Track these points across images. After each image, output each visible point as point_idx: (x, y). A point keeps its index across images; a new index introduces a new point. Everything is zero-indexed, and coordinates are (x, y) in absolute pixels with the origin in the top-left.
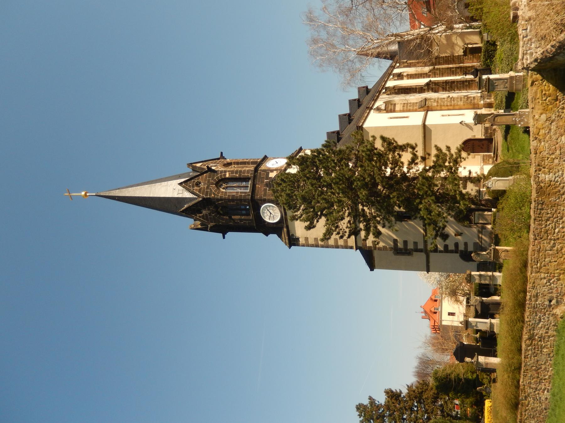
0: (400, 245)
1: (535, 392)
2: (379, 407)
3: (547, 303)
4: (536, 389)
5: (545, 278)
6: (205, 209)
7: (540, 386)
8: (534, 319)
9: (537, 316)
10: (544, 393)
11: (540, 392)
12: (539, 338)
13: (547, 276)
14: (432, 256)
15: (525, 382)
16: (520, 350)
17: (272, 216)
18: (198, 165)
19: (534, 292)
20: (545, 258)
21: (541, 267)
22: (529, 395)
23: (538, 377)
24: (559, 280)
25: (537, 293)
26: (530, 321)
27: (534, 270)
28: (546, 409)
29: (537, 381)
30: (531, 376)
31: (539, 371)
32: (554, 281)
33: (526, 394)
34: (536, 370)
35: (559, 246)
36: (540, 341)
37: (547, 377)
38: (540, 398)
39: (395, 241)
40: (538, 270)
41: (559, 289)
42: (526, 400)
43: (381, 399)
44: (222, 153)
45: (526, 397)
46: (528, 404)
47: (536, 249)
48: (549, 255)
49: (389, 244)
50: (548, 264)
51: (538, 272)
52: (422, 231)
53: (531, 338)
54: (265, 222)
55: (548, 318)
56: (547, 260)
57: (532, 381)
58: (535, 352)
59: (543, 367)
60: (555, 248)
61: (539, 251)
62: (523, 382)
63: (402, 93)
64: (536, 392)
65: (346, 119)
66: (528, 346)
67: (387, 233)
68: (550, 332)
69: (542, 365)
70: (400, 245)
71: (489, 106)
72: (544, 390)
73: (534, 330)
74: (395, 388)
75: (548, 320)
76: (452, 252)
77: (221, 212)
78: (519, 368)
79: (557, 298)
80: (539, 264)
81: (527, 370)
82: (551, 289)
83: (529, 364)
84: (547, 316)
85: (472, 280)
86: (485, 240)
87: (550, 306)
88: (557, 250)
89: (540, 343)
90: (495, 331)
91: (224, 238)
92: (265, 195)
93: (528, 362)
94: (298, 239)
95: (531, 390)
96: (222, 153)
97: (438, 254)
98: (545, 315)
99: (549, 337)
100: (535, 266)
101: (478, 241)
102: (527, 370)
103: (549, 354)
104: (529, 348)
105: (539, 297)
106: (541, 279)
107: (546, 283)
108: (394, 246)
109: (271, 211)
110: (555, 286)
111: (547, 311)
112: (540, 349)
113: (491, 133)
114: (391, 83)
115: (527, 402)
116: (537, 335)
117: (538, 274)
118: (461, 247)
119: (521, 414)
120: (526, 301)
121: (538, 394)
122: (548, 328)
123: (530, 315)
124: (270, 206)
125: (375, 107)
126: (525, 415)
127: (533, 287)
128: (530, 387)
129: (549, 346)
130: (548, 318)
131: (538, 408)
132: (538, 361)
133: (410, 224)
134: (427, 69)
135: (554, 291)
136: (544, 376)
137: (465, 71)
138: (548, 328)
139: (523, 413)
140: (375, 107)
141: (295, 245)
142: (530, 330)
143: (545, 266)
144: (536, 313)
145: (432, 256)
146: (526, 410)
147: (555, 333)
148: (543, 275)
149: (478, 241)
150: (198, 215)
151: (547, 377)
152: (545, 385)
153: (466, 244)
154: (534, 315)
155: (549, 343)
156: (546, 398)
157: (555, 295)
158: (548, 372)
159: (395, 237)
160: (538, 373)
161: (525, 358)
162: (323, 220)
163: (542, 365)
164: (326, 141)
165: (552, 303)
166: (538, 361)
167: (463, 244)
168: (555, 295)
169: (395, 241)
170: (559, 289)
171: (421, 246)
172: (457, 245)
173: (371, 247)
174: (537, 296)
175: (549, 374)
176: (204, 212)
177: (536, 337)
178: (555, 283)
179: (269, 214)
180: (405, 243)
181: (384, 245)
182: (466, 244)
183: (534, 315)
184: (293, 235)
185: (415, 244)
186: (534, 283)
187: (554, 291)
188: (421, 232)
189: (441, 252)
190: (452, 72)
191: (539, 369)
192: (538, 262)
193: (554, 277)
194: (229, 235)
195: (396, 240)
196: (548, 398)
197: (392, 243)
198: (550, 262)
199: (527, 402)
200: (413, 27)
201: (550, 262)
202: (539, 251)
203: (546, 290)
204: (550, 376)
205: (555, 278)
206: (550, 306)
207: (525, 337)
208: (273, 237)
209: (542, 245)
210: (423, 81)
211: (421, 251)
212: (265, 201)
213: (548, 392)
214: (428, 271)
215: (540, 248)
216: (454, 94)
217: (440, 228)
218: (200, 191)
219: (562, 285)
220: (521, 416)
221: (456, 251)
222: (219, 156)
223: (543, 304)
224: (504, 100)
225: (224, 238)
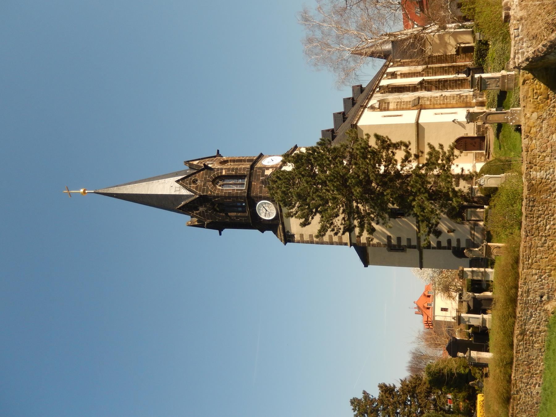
0: (394, 242)
1: (526, 386)
2: (373, 401)
3: (538, 299)
4: (528, 383)
5: (536, 274)
6: (201, 206)
7: (531, 380)
8: (525, 314)
9: (528, 311)
10: (535, 387)
11: (532, 387)
12: (530, 333)
13: (539, 272)
14: (426, 252)
15: (517, 377)
16: (512, 345)
17: (267, 213)
18: (195, 163)
19: (525, 288)
20: (536, 255)
21: (532, 264)
22: (520, 390)
23: (530, 372)
24: (550, 276)
25: (529, 289)
26: (521, 317)
27: (525, 266)
28: (537, 403)
29: (528, 376)
30: (522, 371)
31: (530, 366)
32: (545, 277)
33: (518, 388)
34: (528, 365)
35: (550, 243)
36: (532, 336)
37: (538, 372)
38: (532, 392)
39: (389, 238)
40: (529, 266)
41: (551, 285)
42: (517, 394)
43: (375, 393)
44: (218, 151)
45: (517, 392)
46: (520, 398)
47: (528, 245)
48: (540, 252)
49: (383, 241)
50: (539, 260)
51: (530, 268)
52: (415, 228)
53: (523, 333)
54: (261, 218)
55: (540, 313)
56: (538, 256)
57: (524, 376)
58: (526, 347)
59: (535, 362)
60: (546, 245)
61: (530, 248)
62: (514, 377)
63: (395, 92)
64: (528, 387)
65: (341, 118)
66: (520, 342)
67: (381, 230)
68: (542, 328)
69: (533, 359)
70: (394, 242)
71: (482, 104)
72: (536, 384)
73: (525, 325)
74: (389, 382)
75: (540, 316)
76: (444, 248)
77: (218, 209)
78: (511, 363)
79: (548, 294)
80: (530, 261)
81: (519, 365)
82: (542, 285)
83: (520, 358)
84: (538, 311)
85: (464, 276)
86: (477, 237)
87: (541, 301)
88: (548, 247)
89: (531, 338)
90: (487, 326)
91: (220, 234)
92: (261, 192)
93: (520, 356)
94: (293, 235)
95: (523, 384)
96: (218, 151)
97: (431, 250)
98: (536, 310)
99: (540, 332)
100: (527, 262)
101: (470, 238)
102: (519, 365)
103: (540, 349)
104: (520, 343)
105: (531, 293)
106: (533, 275)
107: (538, 279)
108: (388, 242)
109: (267, 208)
110: (546, 282)
111: (538, 307)
112: (531, 345)
113: (483, 131)
114: (384, 82)
115: (518, 396)
116: (528, 330)
117: (530, 270)
118: (454, 244)
119: (513, 408)
120: (517, 297)
121: (530, 388)
122: (540, 323)
123: (521, 310)
124: (265, 203)
125: (369, 105)
126: (517, 409)
127: (525, 283)
128: (522, 382)
129: (540, 341)
130: (540, 313)
131: (530, 403)
132: (529, 356)
133: (404, 221)
134: (420, 68)
135: (545, 287)
136: (536, 371)
137: (458, 70)
138: (540, 323)
139: (515, 408)
140: (369, 105)
141: (290, 241)
142: (521, 325)
143: (536, 262)
144: (528, 309)
145: (426, 252)
146: (518, 404)
147: (546, 328)
148: (534, 271)
149: (470, 238)
150: (195, 212)
151: (538, 372)
152: (536, 380)
153: (458, 241)
154: (526, 310)
155: (540, 338)
156: (538, 393)
157: (546, 291)
158: (539, 367)
159: (389, 234)
160: (530, 368)
161: (516, 353)
162: (318, 217)
163: (533, 359)
164: (321, 139)
165: (543, 299)
166: (529, 356)
167: (456, 240)
168: (546, 291)
169: (389, 238)
170: (551, 285)
171: (414, 243)
172: (449, 241)
173: (365, 243)
174: (528, 292)
175: (540, 368)
176: (201, 209)
177: (528, 333)
178: (546, 279)
179: (264, 211)
180: (399, 239)
181: (378, 241)
182: (458, 241)
183: (526, 310)
184: (288, 232)
185: (409, 240)
186: (525, 279)
187: (545, 287)
188: (414, 229)
189: (434, 248)
190: (445, 71)
191: (530, 364)
192: (529, 259)
193: (545, 273)
194: (226, 231)
195: (390, 237)
196: (540, 392)
197: (385, 240)
198: (541, 258)
199: (518, 396)
200: (407, 27)
201: (541, 258)
202: (530, 248)
203: (538, 286)
204: (541, 370)
205: (546, 274)
206: (541, 301)
207: (517, 332)
208: (269, 234)
209: (533, 242)
210: (416, 80)
211: (414, 247)
212: (261, 198)
213: (539, 386)
214: (421, 267)
215: (532, 244)
216: (447, 93)
217: (433, 224)
218: (196, 188)
219: (553, 281)
220: (513, 411)
221: (449, 247)
222: (216, 154)
223: (534, 300)
224: (496, 98)
225: (220, 234)
